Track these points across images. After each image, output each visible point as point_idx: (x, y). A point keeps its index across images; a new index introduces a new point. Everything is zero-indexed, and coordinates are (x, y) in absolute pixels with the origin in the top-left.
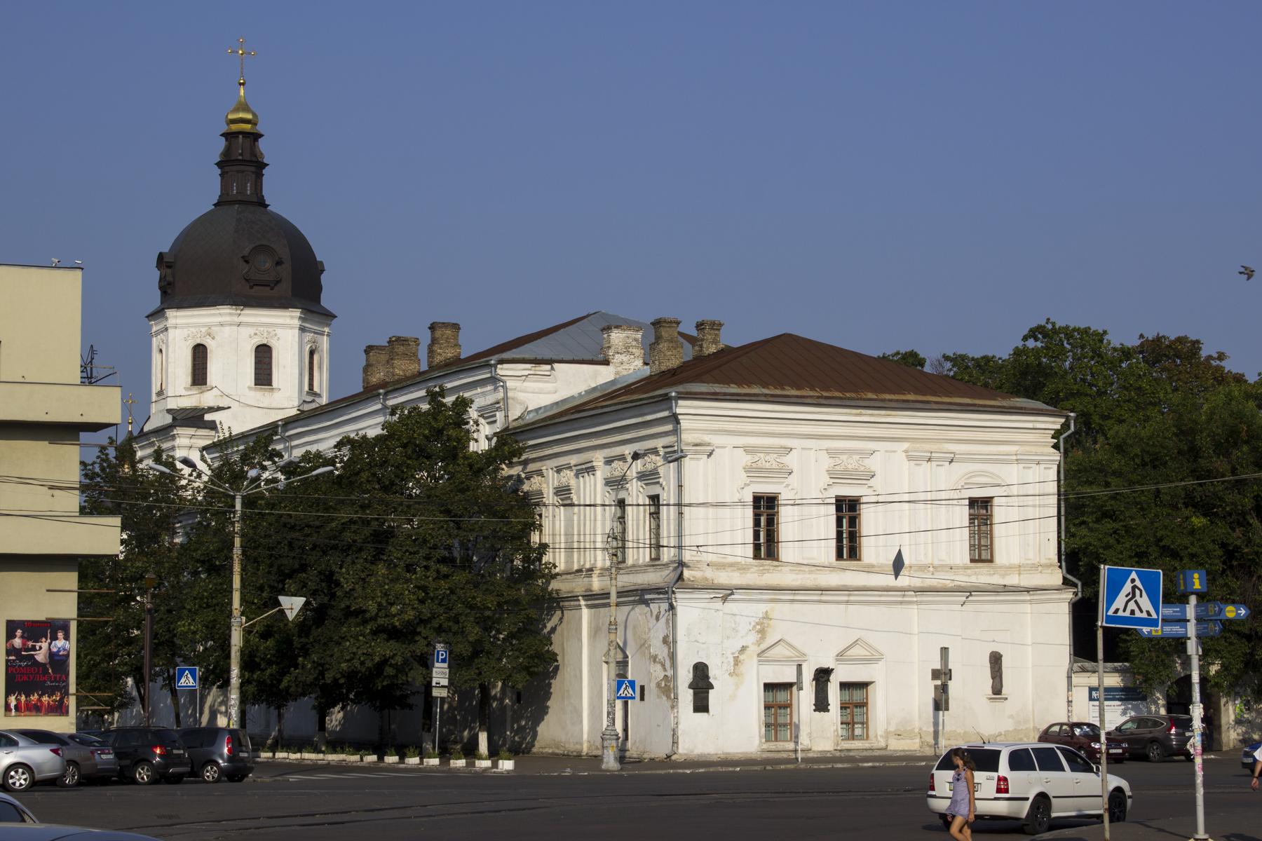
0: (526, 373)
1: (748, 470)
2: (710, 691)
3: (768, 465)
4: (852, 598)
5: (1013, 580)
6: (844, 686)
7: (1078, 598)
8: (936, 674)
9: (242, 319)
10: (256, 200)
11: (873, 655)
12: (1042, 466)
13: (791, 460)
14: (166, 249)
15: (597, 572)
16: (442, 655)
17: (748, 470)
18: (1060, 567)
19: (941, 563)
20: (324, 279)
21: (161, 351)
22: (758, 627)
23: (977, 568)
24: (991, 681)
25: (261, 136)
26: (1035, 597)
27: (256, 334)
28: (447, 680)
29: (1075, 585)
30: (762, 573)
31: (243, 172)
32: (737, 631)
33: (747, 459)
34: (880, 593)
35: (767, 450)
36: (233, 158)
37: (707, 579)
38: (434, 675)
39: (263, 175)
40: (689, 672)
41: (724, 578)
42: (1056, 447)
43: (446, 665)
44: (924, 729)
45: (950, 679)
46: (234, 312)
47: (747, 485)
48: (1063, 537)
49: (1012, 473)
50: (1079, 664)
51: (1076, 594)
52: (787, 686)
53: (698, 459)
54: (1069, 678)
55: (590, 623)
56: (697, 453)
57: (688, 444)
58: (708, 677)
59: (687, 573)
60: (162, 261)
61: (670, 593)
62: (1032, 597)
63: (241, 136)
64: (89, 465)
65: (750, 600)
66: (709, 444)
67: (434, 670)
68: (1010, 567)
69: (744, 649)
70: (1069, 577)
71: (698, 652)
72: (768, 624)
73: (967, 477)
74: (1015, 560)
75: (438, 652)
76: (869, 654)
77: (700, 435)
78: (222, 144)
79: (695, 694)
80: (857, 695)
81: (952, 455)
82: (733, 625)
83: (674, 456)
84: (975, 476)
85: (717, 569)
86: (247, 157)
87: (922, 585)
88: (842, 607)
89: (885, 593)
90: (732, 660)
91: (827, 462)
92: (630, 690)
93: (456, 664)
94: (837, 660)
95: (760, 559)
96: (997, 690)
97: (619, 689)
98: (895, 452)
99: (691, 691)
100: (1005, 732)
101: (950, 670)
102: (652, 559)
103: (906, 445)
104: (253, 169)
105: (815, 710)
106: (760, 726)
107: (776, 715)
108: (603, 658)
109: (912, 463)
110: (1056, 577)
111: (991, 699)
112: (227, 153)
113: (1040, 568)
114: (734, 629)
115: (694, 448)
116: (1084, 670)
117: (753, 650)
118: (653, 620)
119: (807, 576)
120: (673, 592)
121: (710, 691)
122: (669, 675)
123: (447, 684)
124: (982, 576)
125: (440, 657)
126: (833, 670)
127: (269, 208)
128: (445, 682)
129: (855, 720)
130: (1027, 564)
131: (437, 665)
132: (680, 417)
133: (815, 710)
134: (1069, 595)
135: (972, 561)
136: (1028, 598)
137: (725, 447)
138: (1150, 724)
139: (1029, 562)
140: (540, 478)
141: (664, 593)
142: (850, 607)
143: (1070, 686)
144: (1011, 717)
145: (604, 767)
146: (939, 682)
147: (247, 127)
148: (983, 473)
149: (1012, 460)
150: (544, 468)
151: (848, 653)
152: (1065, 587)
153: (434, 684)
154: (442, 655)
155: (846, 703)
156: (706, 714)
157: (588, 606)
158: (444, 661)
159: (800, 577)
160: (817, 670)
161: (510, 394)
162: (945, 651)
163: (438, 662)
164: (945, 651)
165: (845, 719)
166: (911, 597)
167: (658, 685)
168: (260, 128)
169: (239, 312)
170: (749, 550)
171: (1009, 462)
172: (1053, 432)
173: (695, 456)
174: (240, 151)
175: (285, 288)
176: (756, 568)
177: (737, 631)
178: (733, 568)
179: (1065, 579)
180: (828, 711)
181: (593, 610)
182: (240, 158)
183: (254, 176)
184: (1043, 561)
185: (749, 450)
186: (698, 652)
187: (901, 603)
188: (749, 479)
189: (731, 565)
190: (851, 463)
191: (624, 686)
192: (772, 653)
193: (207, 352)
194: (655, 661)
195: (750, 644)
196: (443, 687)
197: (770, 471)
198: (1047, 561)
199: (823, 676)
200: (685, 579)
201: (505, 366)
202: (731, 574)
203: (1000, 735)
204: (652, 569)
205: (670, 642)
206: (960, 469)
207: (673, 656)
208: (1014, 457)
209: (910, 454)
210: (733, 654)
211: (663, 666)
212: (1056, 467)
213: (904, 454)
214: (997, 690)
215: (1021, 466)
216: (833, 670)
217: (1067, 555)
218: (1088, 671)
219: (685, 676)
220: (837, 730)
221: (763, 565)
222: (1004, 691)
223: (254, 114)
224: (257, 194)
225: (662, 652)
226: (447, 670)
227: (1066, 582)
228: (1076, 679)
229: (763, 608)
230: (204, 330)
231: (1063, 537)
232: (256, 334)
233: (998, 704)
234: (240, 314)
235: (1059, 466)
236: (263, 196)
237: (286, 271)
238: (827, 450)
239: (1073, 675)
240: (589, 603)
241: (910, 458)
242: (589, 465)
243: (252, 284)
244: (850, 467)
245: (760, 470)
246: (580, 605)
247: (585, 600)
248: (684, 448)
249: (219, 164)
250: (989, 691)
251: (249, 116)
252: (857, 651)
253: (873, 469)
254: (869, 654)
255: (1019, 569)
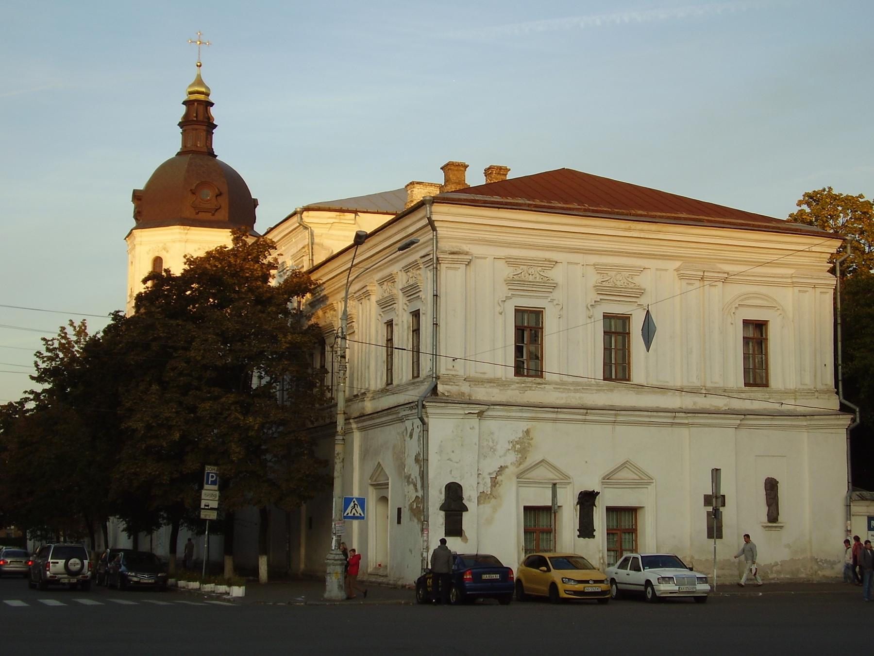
0: (331, 221)
1: (510, 282)
2: (464, 513)
3: (531, 278)
4: (620, 419)
5: (789, 406)
6: (610, 510)
7: (855, 424)
8: (708, 500)
9: (188, 237)
10: (206, 151)
11: (642, 479)
12: (818, 291)
13: (557, 274)
14: (141, 186)
15: (369, 395)
16: (212, 477)
17: (510, 282)
18: (837, 393)
19: (713, 385)
20: (258, 211)
21: (132, 262)
22: (518, 446)
23: (752, 392)
24: (767, 508)
25: (212, 104)
26: (812, 423)
27: (199, 249)
28: (217, 503)
29: (852, 411)
30: (524, 390)
31: (197, 129)
32: (495, 450)
33: (508, 271)
34: (649, 413)
35: (530, 263)
36: (190, 119)
37: (463, 394)
38: (203, 497)
39: (213, 133)
40: (441, 493)
41: (481, 393)
42: (832, 271)
43: (216, 487)
44: (696, 557)
45: (724, 505)
46: (182, 231)
47: (508, 298)
48: (840, 362)
49: (787, 297)
50: (858, 493)
51: (854, 420)
52: (547, 510)
53: (455, 269)
54: (848, 506)
55: (361, 446)
56: (454, 262)
57: (444, 252)
58: (461, 498)
59: (440, 388)
60: (137, 196)
61: (420, 407)
62: (809, 422)
63: (196, 104)
64: (49, 341)
65: (508, 418)
66: (467, 253)
67: (203, 492)
68: (786, 392)
69: (502, 469)
70: (846, 403)
71: (451, 471)
72: (529, 444)
73: (741, 298)
74: (792, 385)
75: (208, 474)
76: (637, 477)
77: (458, 244)
78: (184, 109)
79: (447, 517)
80: (626, 523)
81: (726, 276)
82: (491, 444)
83: (435, 264)
84: (748, 298)
85: (475, 385)
86: (201, 118)
87: (694, 407)
88: (609, 427)
89: (655, 414)
90: (489, 481)
91: (594, 278)
92: (359, 509)
93: (224, 486)
94: (603, 483)
95: (523, 375)
96: (773, 517)
97: (345, 509)
98: (666, 270)
99: (443, 513)
100: (782, 561)
101: (724, 496)
102: (413, 377)
103: (677, 264)
104: (204, 127)
105: (579, 536)
106: (519, 552)
107: (538, 541)
108: (370, 481)
109: (684, 282)
110: (834, 403)
111: (767, 527)
112: (186, 117)
113: (816, 394)
114: (491, 448)
115: (450, 256)
116: (863, 498)
117: (512, 470)
118: (407, 438)
119: (572, 394)
120: (424, 406)
121: (464, 513)
122: (420, 496)
123: (216, 507)
124: (756, 401)
125: (210, 479)
126: (598, 493)
127: (217, 158)
128: (215, 504)
129: (623, 547)
130: (803, 389)
131: (206, 486)
132: (436, 224)
133: (579, 536)
134: (846, 420)
135: (746, 385)
136: (805, 423)
137: (485, 258)
138: (79, 587)
139: (805, 387)
140: (332, 312)
141: (419, 407)
142: (618, 428)
143: (849, 515)
144: (788, 546)
145: (326, 595)
146: (710, 509)
147: (202, 97)
148: (757, 296)
149: (786, 283)
150: (335, 302)
151: (615, 476)
152: (842, 413)
153: (203, 506)
154: (212, 477)
155: (612, 529)
156: (459, 538)
157: (359, 429)
158: (214, 483)
159: (564, 395)
160: (581, 493)
161: (316, 240)
162: (716, 473)
163: (207, 483)
164: (716, 473)
165: (611, 546)
166: (681, 419)
167: (411, 509)
168: (211, 98)
169: (186, 231)
170: (512, 371)
171: (784, 285)
172: (829, 256)
173: (452, 266)
174: (195, 115)
175: (223, 215)
176: (519, 385)
177: (495, 450)
178: (492, 384)
179: (841, 404)
180: (594, 537)
181: (363, 432)
182: (195, 119)
183: (205, 133)
184: (820, 386)
185: (510, 261)
186: (451, 471)
187: (672, 424)
188: (511, 292)
189: (490, 381)
190: (620, 280)
191: (352, 504)
192: (535, 474)
193: (162, 262)
194: (408, 482)
195: (509, 464)
196: (212, 509)
197: (533, 284)
198: (823, 387)
199: (587, 500)
200: (439, 394)
201: (311, 213)
202: (490, 390)
203: (776, 564)
204: (411, 387)
205: (422, 461)
206: (734, 290)
207: (424, 475)
208: (789, 280)
209: (682, 272)
210: (490, 474)
211: (415, 485)
212: (832, 291)
213: (676, 273)
214: (773, 517)
215: (796, 289)
216: (598, 493)
217: (843, 380)
218: (867, 500)
219: (436, 497)
220: (603, 557)
221: (524, 382)
222: (780, 518)
223: (207, 88)
224: (207, 147)
225: (414, 471)
226: (217, 493)
227: (844, 409)
228: (855, 509)
229: (524, 425)
230: (161, 245)
231: (840, 362)
232: (199, 249)
233: (774, 533)
234: (187, 233)
235: (835, 289)
236: (213, 149)
237: (224, 201)
238: (594, 265)
239: (852, 504)
240: (360, 425)
241: (682, 277)
242: (364, 290)
243: (197, 211)
244: (618, 283)
245: (522, 282)
246: (351, 428)
247: (357, 423)
248: (441, 256)
249: (181, 125)
250: (764, 518)
251: (203, 90)
252: (625, 474)
253: (643, 286)
254: (637, 477)
255: (795, 394)
